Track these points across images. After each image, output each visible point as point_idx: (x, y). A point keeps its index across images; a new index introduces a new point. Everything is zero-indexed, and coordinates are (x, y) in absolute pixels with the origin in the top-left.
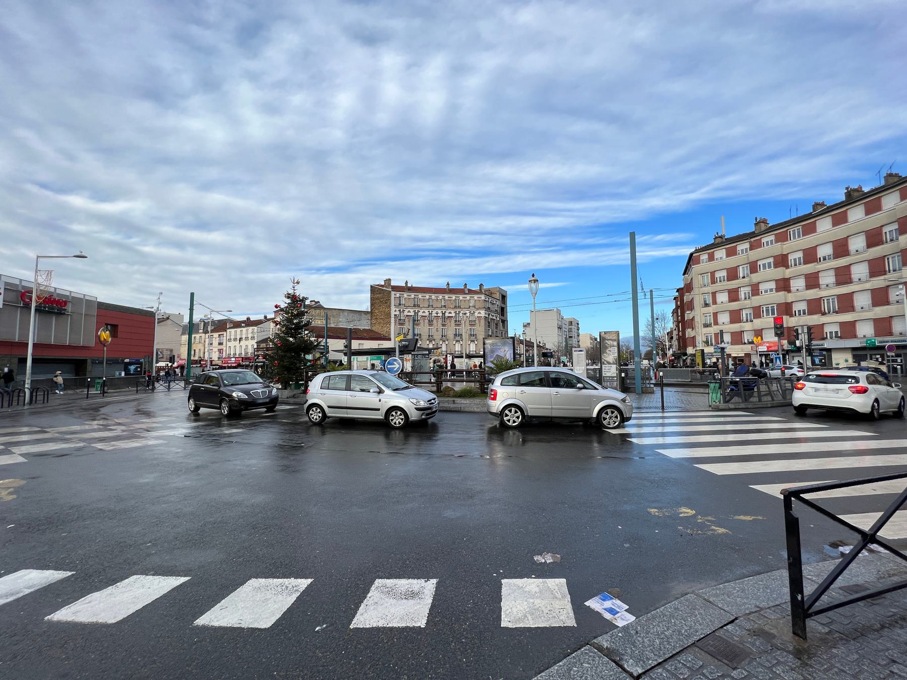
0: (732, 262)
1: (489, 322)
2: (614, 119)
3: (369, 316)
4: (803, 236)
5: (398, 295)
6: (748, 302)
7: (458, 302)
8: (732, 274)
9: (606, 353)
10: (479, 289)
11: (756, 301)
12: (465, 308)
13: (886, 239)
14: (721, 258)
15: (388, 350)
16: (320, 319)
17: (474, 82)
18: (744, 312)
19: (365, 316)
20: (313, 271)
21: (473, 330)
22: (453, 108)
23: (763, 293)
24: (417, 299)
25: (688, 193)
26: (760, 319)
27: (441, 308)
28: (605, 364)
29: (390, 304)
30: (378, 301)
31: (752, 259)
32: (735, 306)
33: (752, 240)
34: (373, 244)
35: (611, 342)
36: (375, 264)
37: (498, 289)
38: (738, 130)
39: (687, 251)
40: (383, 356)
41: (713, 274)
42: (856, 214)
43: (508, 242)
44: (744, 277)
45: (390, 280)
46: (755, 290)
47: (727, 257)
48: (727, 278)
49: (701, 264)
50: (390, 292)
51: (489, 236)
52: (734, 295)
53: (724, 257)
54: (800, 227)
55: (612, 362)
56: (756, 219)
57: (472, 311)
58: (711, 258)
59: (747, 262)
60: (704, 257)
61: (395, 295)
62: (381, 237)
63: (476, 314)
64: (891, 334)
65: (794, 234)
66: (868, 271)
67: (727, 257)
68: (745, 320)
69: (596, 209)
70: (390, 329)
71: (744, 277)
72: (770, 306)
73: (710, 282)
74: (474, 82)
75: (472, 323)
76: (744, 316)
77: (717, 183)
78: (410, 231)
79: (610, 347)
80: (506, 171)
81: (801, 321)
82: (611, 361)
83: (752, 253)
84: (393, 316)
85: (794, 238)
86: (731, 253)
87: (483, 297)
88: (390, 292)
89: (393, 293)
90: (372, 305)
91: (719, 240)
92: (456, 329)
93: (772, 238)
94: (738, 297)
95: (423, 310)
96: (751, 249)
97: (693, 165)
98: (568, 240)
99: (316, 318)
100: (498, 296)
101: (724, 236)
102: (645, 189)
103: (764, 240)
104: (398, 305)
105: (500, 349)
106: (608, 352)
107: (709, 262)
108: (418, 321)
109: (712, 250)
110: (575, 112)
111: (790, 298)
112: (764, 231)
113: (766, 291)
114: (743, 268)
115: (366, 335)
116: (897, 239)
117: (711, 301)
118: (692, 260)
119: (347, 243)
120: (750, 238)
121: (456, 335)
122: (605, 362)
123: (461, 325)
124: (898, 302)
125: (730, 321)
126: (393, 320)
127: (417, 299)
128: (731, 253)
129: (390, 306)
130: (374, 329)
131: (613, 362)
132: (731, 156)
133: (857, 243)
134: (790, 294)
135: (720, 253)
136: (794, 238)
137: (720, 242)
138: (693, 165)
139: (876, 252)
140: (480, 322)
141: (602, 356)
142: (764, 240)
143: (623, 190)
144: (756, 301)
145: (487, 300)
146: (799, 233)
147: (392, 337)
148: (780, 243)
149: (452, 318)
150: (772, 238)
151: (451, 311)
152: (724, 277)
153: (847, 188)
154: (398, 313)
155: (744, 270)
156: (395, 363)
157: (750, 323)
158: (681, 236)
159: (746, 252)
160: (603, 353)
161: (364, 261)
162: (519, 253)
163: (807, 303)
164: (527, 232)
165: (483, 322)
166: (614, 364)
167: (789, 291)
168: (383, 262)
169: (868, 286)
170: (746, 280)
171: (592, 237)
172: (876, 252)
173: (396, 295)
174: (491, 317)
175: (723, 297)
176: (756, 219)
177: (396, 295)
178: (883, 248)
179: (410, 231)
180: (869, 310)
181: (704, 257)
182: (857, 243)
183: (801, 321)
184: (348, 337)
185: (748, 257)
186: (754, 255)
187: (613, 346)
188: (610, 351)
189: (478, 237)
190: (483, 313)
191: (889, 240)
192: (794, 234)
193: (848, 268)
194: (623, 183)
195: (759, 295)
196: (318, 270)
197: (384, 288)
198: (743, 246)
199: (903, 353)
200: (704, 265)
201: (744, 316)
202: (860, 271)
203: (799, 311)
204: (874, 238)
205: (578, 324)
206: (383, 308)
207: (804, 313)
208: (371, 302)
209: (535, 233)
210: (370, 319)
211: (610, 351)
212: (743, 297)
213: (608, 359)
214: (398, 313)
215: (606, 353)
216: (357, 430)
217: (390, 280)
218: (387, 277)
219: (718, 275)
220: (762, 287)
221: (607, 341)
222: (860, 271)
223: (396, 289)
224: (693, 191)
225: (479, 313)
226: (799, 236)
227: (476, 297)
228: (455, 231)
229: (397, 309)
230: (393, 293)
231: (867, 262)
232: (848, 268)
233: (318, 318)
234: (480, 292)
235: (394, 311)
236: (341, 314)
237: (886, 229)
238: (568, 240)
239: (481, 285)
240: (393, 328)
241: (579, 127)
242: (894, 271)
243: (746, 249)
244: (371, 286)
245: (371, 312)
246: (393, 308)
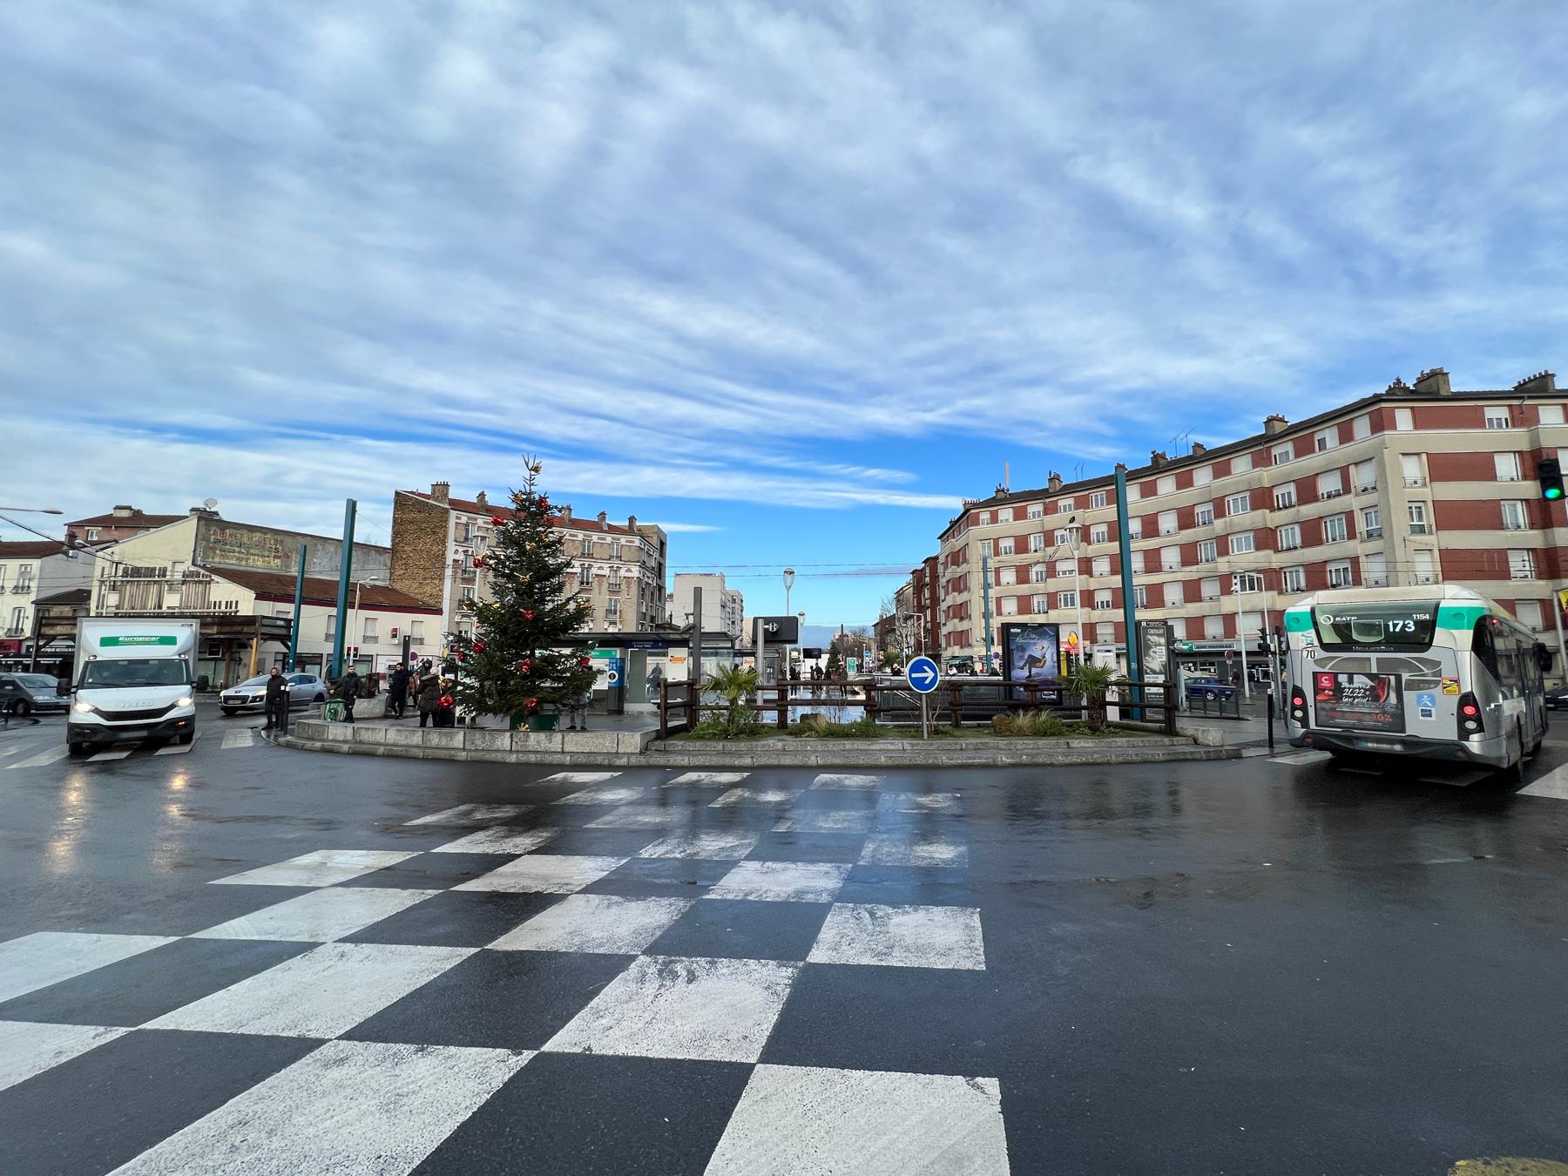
0: (1021, 527)
1: (643, 590)
2: (858, 267)
3: (387, 558)
4: (1108, 504)
5: (464, 520)
6: (1041, 585)
7: (589, 546)
8: (1021, 545)
9: (1149, 656)
10: (628, 524)
11: (1052, 585)
12: (601, 559)
13: (1327, 538)
14: (1007, 520)
15: (630, 636)
16: (262, 556)
17: (647, 116)
18: (1035, 600)
19: (378, 556)
20: (140, 431)
21: (615, 600)
22: (595, 152)
23: (1061, 576)
24: (589, 542)
25: (925, 411)
26: (1057, 611)
27: (609, 559)
28: (1148, 674)
29: (445, 536)
30: (412, 527)
31: (1048, 527)
32: (1024, 589)
33: (1047, 500)
34: (333, 394)
35: (1156, 638)
36: (328, 439)
37: (656, 530)
38: (1005, 334)
39: (955, 504)
40: (618, 650)
41: (996, 541)
42: (1166, 485)
43: (615, 435)
44: (1036, 551)
45: (446, 486)
46: (1051, 571)
47: (1015, 520)
48: (1016, 550)
49: (981, 526)
50: (447, 511)
51: (604, 423)
52: (1023, 575)
53: (1011, 520)
54: (1104, 492)
55: (1157, 670)
56: (1050, 474)
57: (615, 566)
58: (994, 519)
59: (1040, 530)
60: (985, 516)
61: (457, 518)
62: (355, 380)
63: (623, 573)
64: (1203, 637)
65: (1096, 500)
66: (1180, 560)
67: (1015, 520)
68: (1036, 611)
69: (794, 410)
70: (441, 590)
71: (1036, 551)
72: (1069, 593)
73: (992, 552)
74: (647, 116)
75: (614, 589)
76: (1036, 604)
77: (961, 405)
78: (436, 381)
79: (1156, 646)
80: (664, 306)
81: (1106, 616)
82: (1157, 670)
83: (1048, 518)
84: (449, 561)
85: (1097, 506)
86: (1020, 515)
87: (637, 541)
88: (447, 511)
89: (453, 514)
90: (396, 533)
91: (1001, 495)
92: (610, 600)
93: (1071, 501)
94: (1029, 577)
95: (599, 565)
96: (1046, 513)
97: (939, 370)
98: (737, 453)
99: (252, 551)
100: (655, 541)
101: (1008, 490)
102: (872, 392)
103: (1061, 503)
104: (462, 540)
105: (1035, 644)
106: (1152, 654)
107: (991, 523)
108: (587, 584)
109: (996, 508)
110: (803, 234)
111: (1093, 584)
112: (1059, 491)
113: (1064, 573)
114: (1035, 537)
115: (382, 600)
116: (1211, 523)
117: (994, 581)
118: (966, 518)
119: (263, 380)
120: (1046, 498)
121: (608, 611)
122: (1149, 671)
123: (593, 592)
124: (1211, 599)
125: (1018, 611)
126: (449, 572)
127: (589, 542)
128: (1020, 515)
129: (443, 541)
130: (397, 586)
131: (1161, 670)
132: (988, 368)
133: (1168, 522)
134: (1092, 579)
135: (1006, 513)
136: (1097, 506)
137: (1001, 499)
138: (939, 370)
139: (1188, 535)
140: (628, 587)
141: (1145, 663)
142: (1061, 503)
143: (841, 387)
144: (1052, 585)
145: (642, 547)
146: (1102, 499)
147: (446, 606)
148: (1082, 510)
149: (604, 579)
150: (1071, 501)
151: (602, 565)
152: (1010, 547)
153: (1153, 453)
154: (461, 557)
155: (1035, 541)
156: (926, 668)
157: (1044, 615)
158: (898, 475)
159: (1039, 516)
160: (1145, 656)
161: (298, 427)
162: (651, 463)
163: (1113, 593)
164: (677, 427)
165: (634, 588)
166: (1161, 673)
167: (1091, 575)
168: (349, 437)
169: (1179, 576)
170: (1039, 554)
171: (778, 455)
172: (1188, 535)
173: (459, 518)
174: (646, 580)
175: (1009, 577)
176: (1050, 474)
177: (459, 518)
178: (1195, 532)
179: (436, 381)
180: (1182, 607)
181: (985, 516)
182: (1168, 522)
183: (1106, 616)
184: (341, 601)
185: (1043, 524)
186: (1051, 521)
187: (1160, 645)
188: (1155, 652)
189: (579, 420)
190: (635, 572)
191: (1200, 524)
192: (1096, 500)
193: (1157, 551)
194: (843, 376)
195: (1055, 577)
196: (158, 430)
197: (430, 501)
198: (1035, 508)
199: (1218, 662)
200: (983, 528)
201: (1036, 604)
202: (1170, 557)
203: (1102, 602)
204: (1186, 519)
205: (742, 601)
206: (426, 543)
207: (1108, 606)
208: (394, 527)
209: (688, 432)
210: (389, 564)
211: (1155, 652)
212: (1034, 578)
213: (1151, 666)
214: (461, 557)
215: (1149, 656)
216: (1320, 761)
217: (446, 486)
218: (441, 480)
219: (1003, 544)
220: (1060, 567)
221: (1149, 637)
222: (1170, 557)
223: (459, 505)
224: (930, 410)
225: (629, 570)
226: (1102, 505)
227: (623, 540)
228: (534, 401)
229: (461, 549)
230: (453, 514)
231: (1349, 560)
232: (1157, 551)
233: (257, 552)
234: (630, 530)
235: (453, 552)
236: (320, 547)
237: (1198, 510)
238: (737, 453)
239: (632, 519)
240: (449, 591)
241: (805, 262)
242: (1208, 561)
243: (1039, 512)
244: (397, 494)
245: (394, 551)
246: (451, 546)
